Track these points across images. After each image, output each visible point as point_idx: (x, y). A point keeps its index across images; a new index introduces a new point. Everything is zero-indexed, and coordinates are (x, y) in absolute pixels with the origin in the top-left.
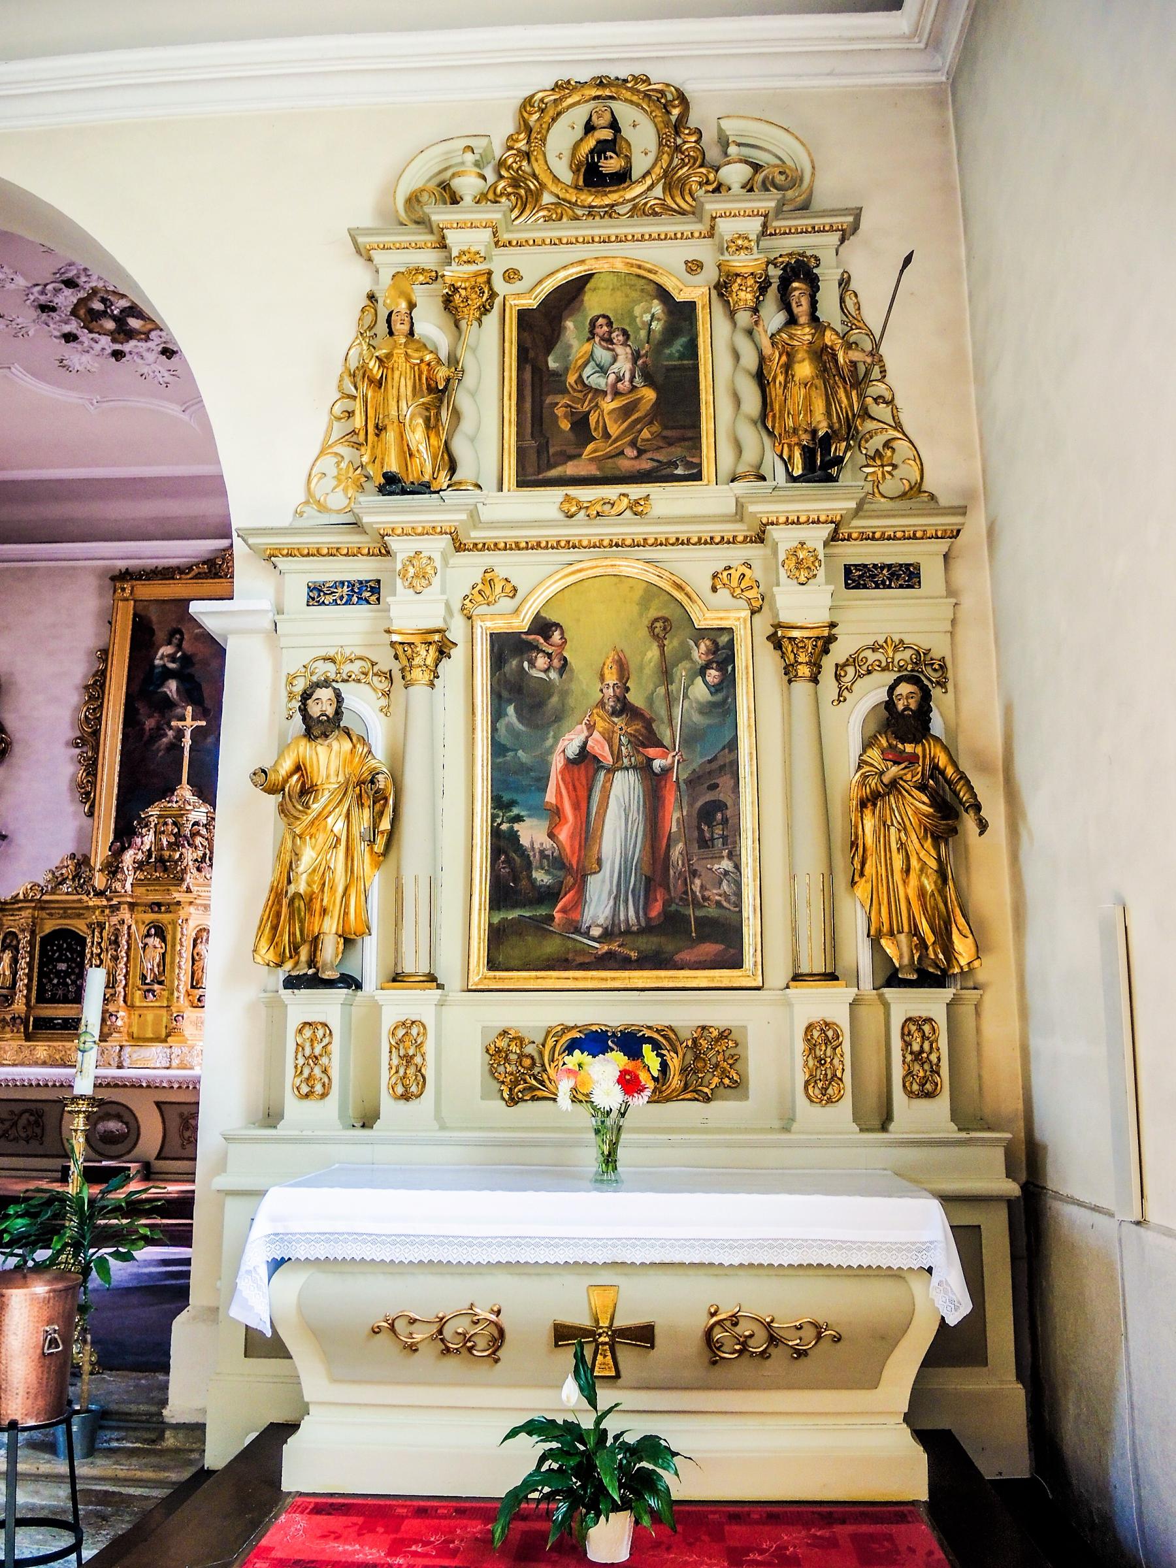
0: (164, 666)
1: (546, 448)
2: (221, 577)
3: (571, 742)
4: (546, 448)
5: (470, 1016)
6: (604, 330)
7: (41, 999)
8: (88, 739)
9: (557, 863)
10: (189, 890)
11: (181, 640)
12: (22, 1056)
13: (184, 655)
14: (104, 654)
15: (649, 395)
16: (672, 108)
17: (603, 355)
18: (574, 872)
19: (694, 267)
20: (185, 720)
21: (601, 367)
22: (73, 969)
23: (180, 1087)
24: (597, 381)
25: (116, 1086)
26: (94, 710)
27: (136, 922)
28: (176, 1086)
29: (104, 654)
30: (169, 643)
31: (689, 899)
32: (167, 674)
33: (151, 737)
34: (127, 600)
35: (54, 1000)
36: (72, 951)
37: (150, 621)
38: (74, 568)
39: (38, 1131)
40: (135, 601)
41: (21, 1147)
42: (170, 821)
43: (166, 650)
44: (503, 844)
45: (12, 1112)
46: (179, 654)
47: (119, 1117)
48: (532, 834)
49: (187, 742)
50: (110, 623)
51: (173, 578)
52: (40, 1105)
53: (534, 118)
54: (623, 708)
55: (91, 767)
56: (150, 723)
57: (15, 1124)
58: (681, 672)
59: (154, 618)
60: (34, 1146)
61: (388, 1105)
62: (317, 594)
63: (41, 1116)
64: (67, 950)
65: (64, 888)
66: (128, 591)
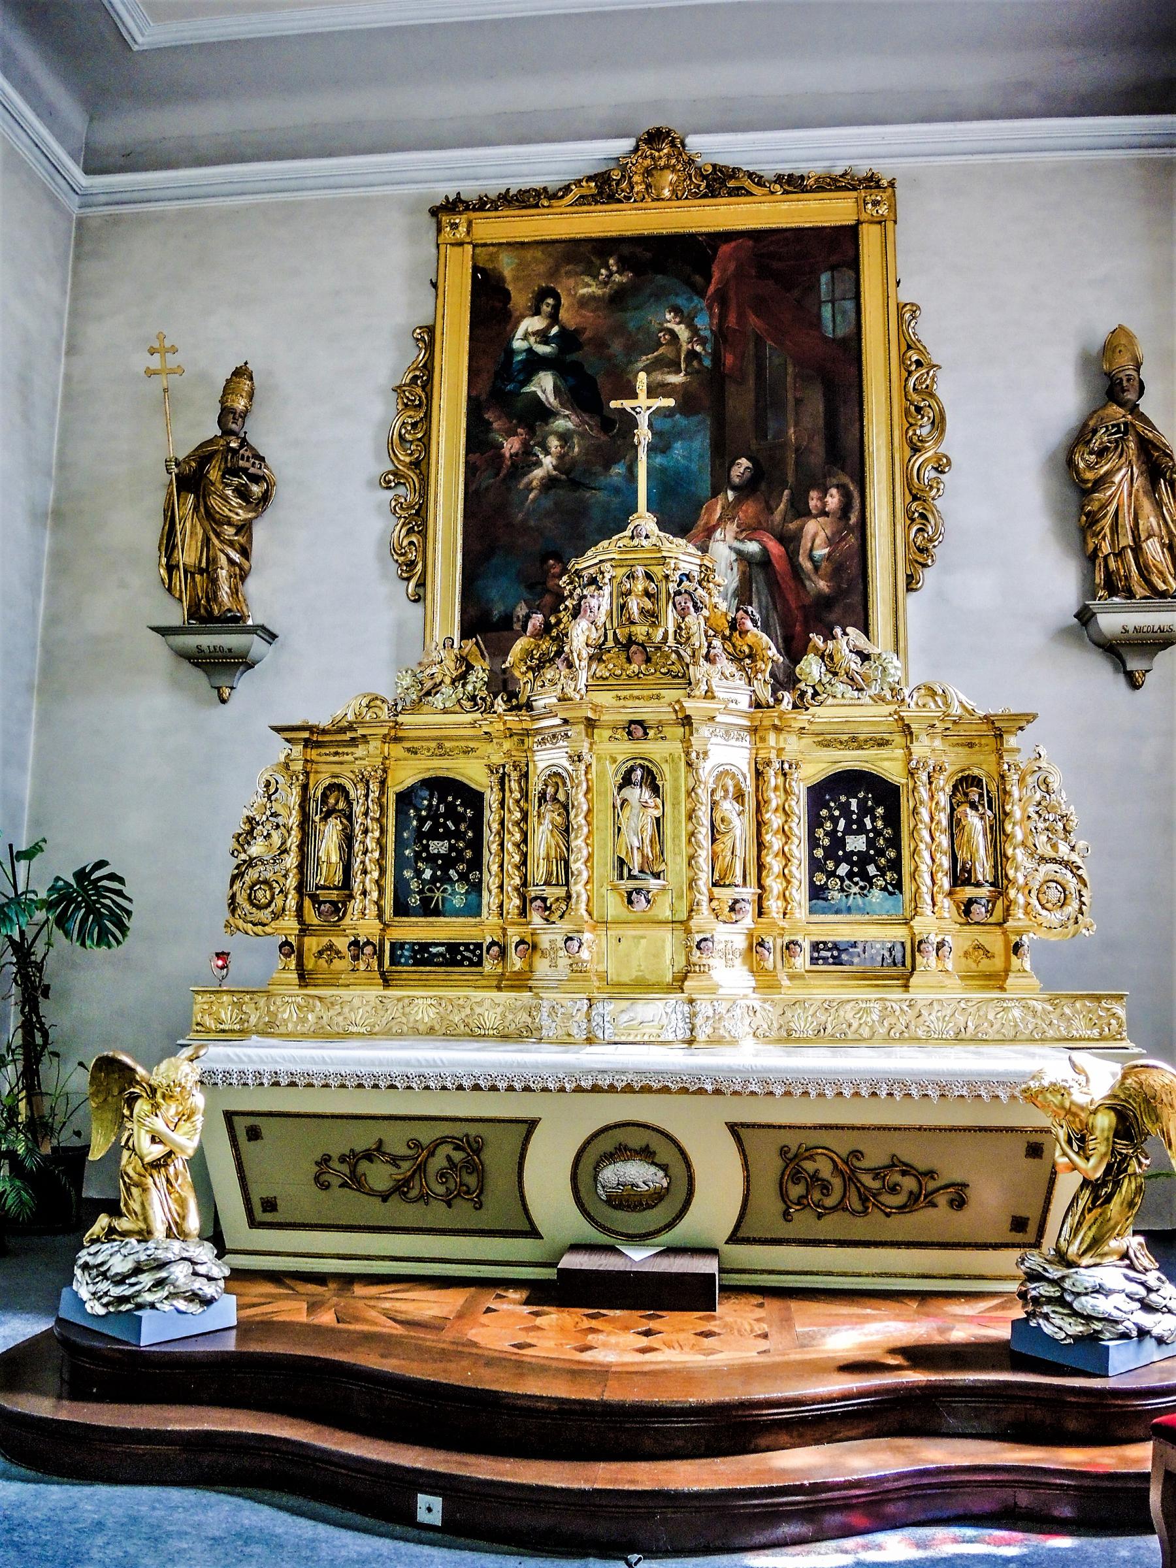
0: (530, 350)
2: (619, 201)
7: (401, 909)
8: (411, 469)
10: (709, 695)
11: (557, 307)
12: (388, 1016)
13: (563, 330)
14: (428, 337)
20: (635, 396)
22: (460, 852)
23: (788, 1094)
25: (646, 1089)
26: (414, 425)
27: (599, 759)
28: (779, 1090)
29: (428, 337)
30: (537, 312)
32: (534, 363)
33: (514, 465)
34: (461, 244)
36: (458, 819)
37: (501, 279)
38: (366, 200)
39: (471, 1181)
40: (475, 246)
41: (438, 1214)
42: (640, 571)
45: (418, 1145)
46: (555, 330)
47: (646, 1154)
50: (435, 285)
51: (536, 206)
52: (473, 1130)
55: (417, 519)
56: (511, 446)
57: (421, 1169)
59: (507, 273)
60: (463, 1214)
63: (478, 1151)
64: (446, 816)
65: (438, 701)
66: (463, 229)
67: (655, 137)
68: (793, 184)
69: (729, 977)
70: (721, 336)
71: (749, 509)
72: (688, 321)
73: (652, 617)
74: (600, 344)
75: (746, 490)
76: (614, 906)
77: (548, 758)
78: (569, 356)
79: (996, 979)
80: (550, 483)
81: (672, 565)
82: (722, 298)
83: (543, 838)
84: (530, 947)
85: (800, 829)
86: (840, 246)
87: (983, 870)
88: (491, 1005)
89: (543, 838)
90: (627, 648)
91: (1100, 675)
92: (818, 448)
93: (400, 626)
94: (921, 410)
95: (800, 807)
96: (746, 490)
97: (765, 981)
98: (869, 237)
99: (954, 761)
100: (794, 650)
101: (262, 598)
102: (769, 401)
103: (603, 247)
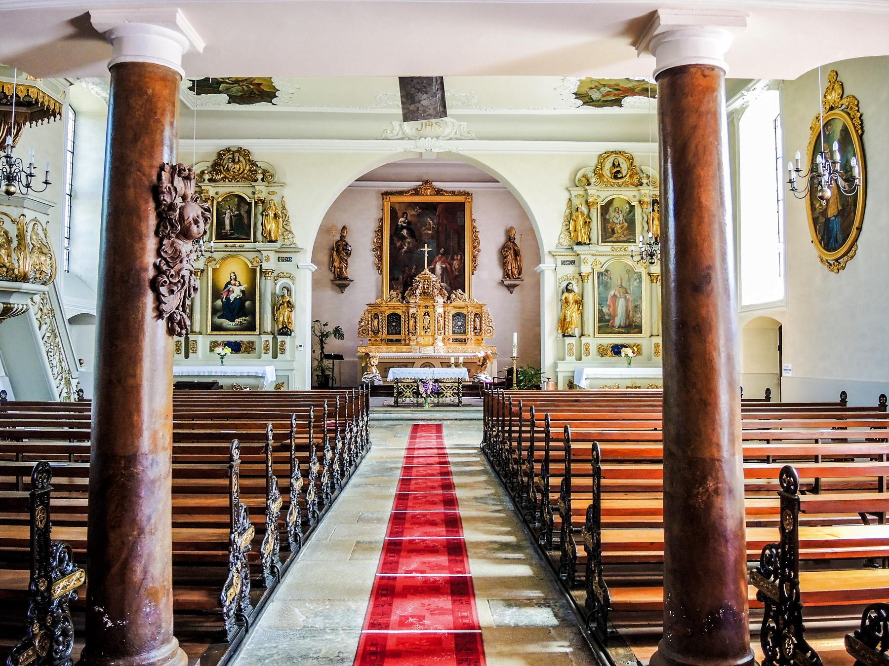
1: (608, 234)
3: (612, 293)
4: (608, 234)
5: (595, 341)
6: (617, 210)
8: (379, 247)
9: (610, 315)
15: (626, 224)
16: (630, 159)
17: (617, 216)
18: (613, 316)
19: (634, 196)
21: (617, 218)
24: (616, 221)
29: (382, 220)
31: (633, 321)
32: (403, 228)
35: (392, 334)
43: (402, 219)
44: (600, 311)
48: (605, 310)
49: (426, 255)
53: (602, 158)
54: (621, 287)
55: (380, 258)
56: (398, 244)
58: (632, 280)
61: (583, 356)
62: (563, 263)
67: (426, 182)
68: (453, 193)
69: (440, 344)
70: (438, 224)
71: (443, 259)
72: (432, 220)
73: (428, 288)
74: (416, 224)
75: (443, 255)
76: (423, 333)
77: (412, 311)
78: (409, 226)
79: (480, 344)
80: (406, 252)
81: (430, 277)
82: (439, 216)
83: (412, 322)
84: (410, 339)
85: (451, 321)
86: (461, 207)
87: (478, 328)
88: (404, 348)
89: (412, 322)
90: (424, 293)
91: (505, 292)
92: (456, 246)
93: (377, 279)
94: (475, 241)
95: (451, 318)
96: (443, 255)
97: (445, 344)
98: (467, 205)
99: (475, 311)
100: (450, 293)
101: (350, 273)
102: (447, 237)
103: (416, 204)
